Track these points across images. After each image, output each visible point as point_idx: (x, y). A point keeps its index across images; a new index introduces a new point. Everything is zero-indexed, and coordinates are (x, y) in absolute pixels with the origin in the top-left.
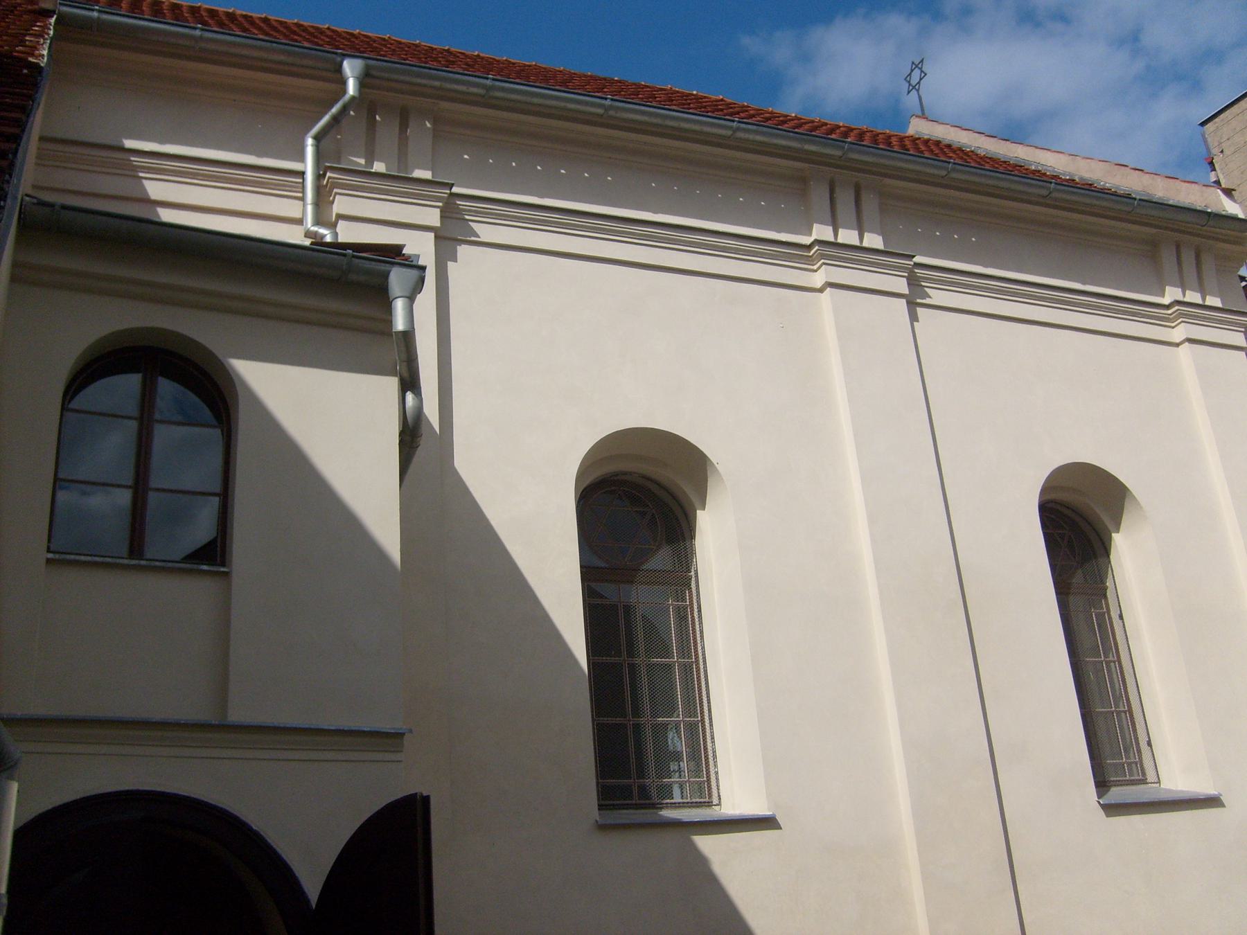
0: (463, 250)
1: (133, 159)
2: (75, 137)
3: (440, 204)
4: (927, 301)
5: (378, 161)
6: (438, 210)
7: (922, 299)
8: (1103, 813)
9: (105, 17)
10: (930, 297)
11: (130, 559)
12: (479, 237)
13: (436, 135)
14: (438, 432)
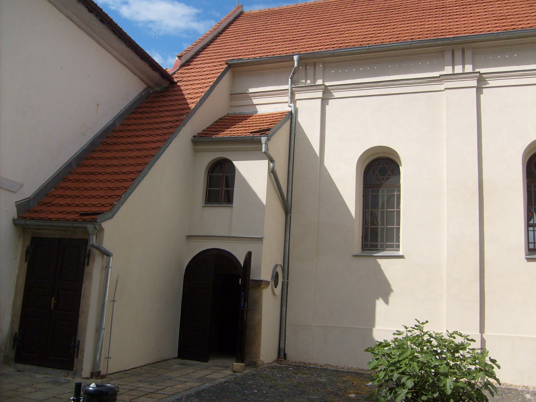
0: (330, 101)
1: (483, 76)
2: (238, 92)
3: (477, 79)
4: (488, 86)
5: (456, 65)
6: (322, 92)
7: (485, 85)
8: (526, 260)
9: (238, 62)
10: (489, 84)
11: (229, 190)
12: (334, 96)
13: (324, 68)
14: (318, 155)
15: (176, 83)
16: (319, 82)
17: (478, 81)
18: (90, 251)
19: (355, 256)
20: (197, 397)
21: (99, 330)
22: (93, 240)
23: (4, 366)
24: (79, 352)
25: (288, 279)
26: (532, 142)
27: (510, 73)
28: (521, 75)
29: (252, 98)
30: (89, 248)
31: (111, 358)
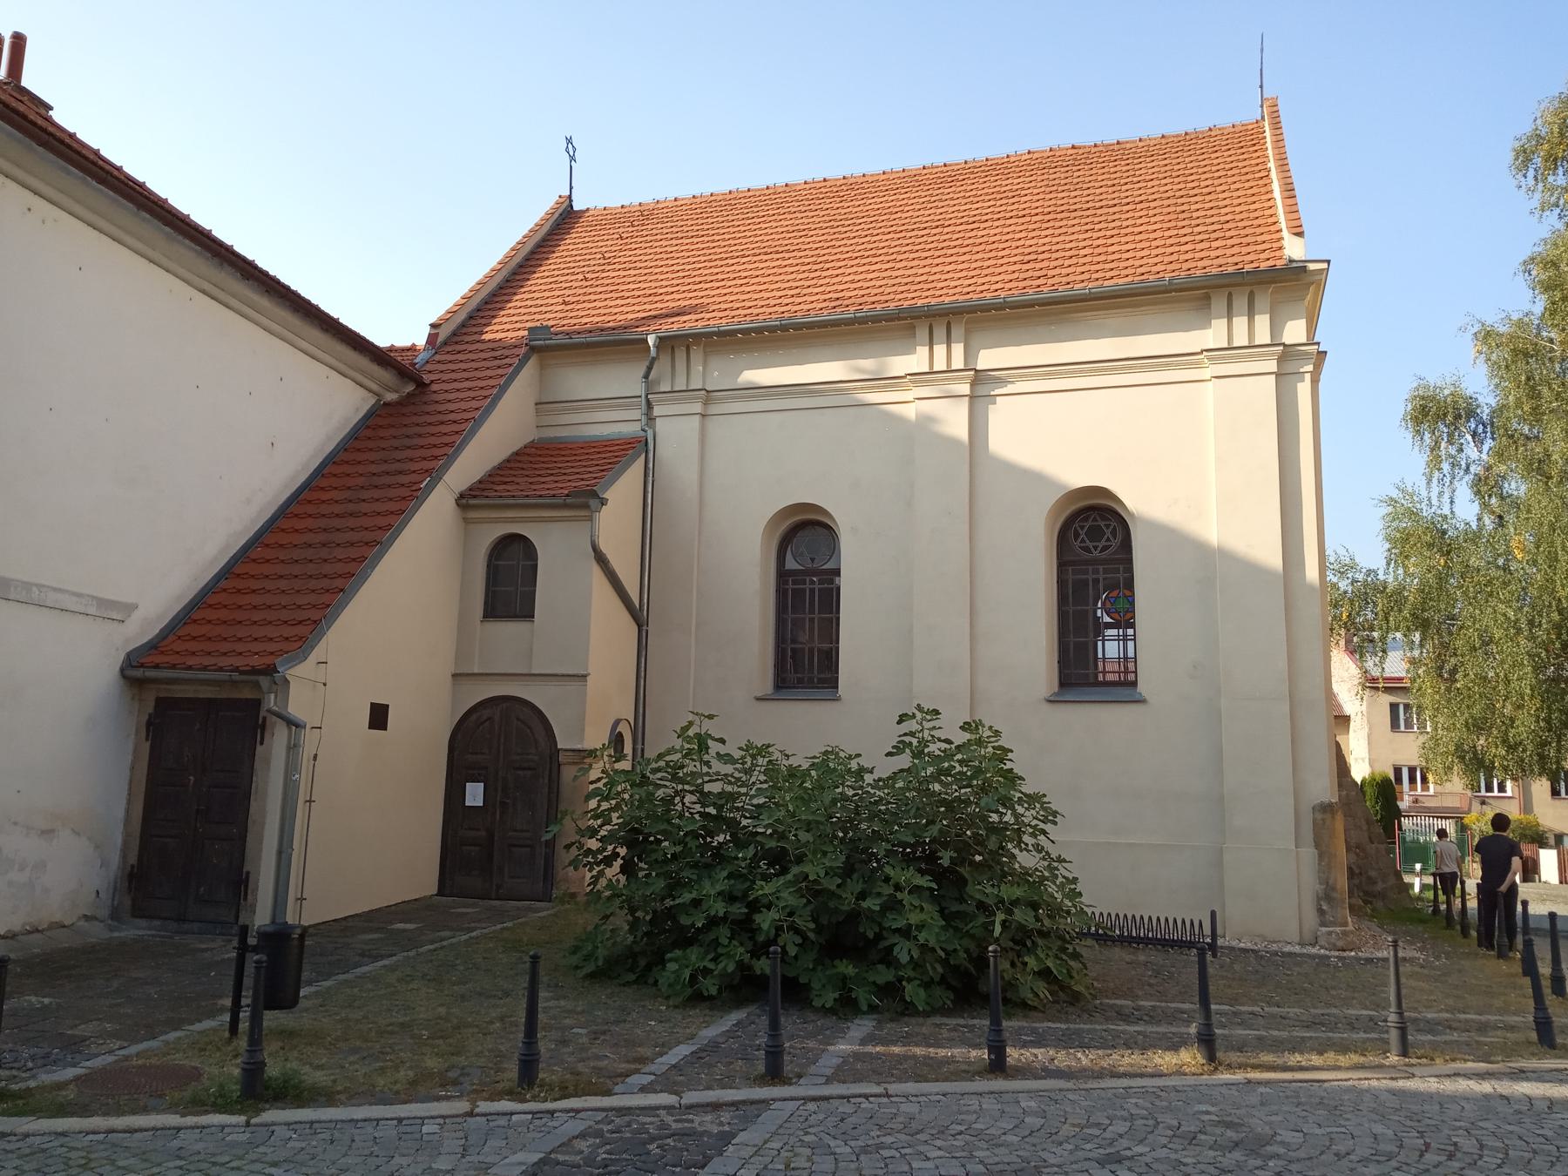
15: (428, 385)
17: (973, 384)
18: (264, 718)
19: (758, 699)
20: (946, 765)
21: (283, 854)
22: (271, 702)
24: (249, 892)
25: (643, 744)
30: (262, 714)
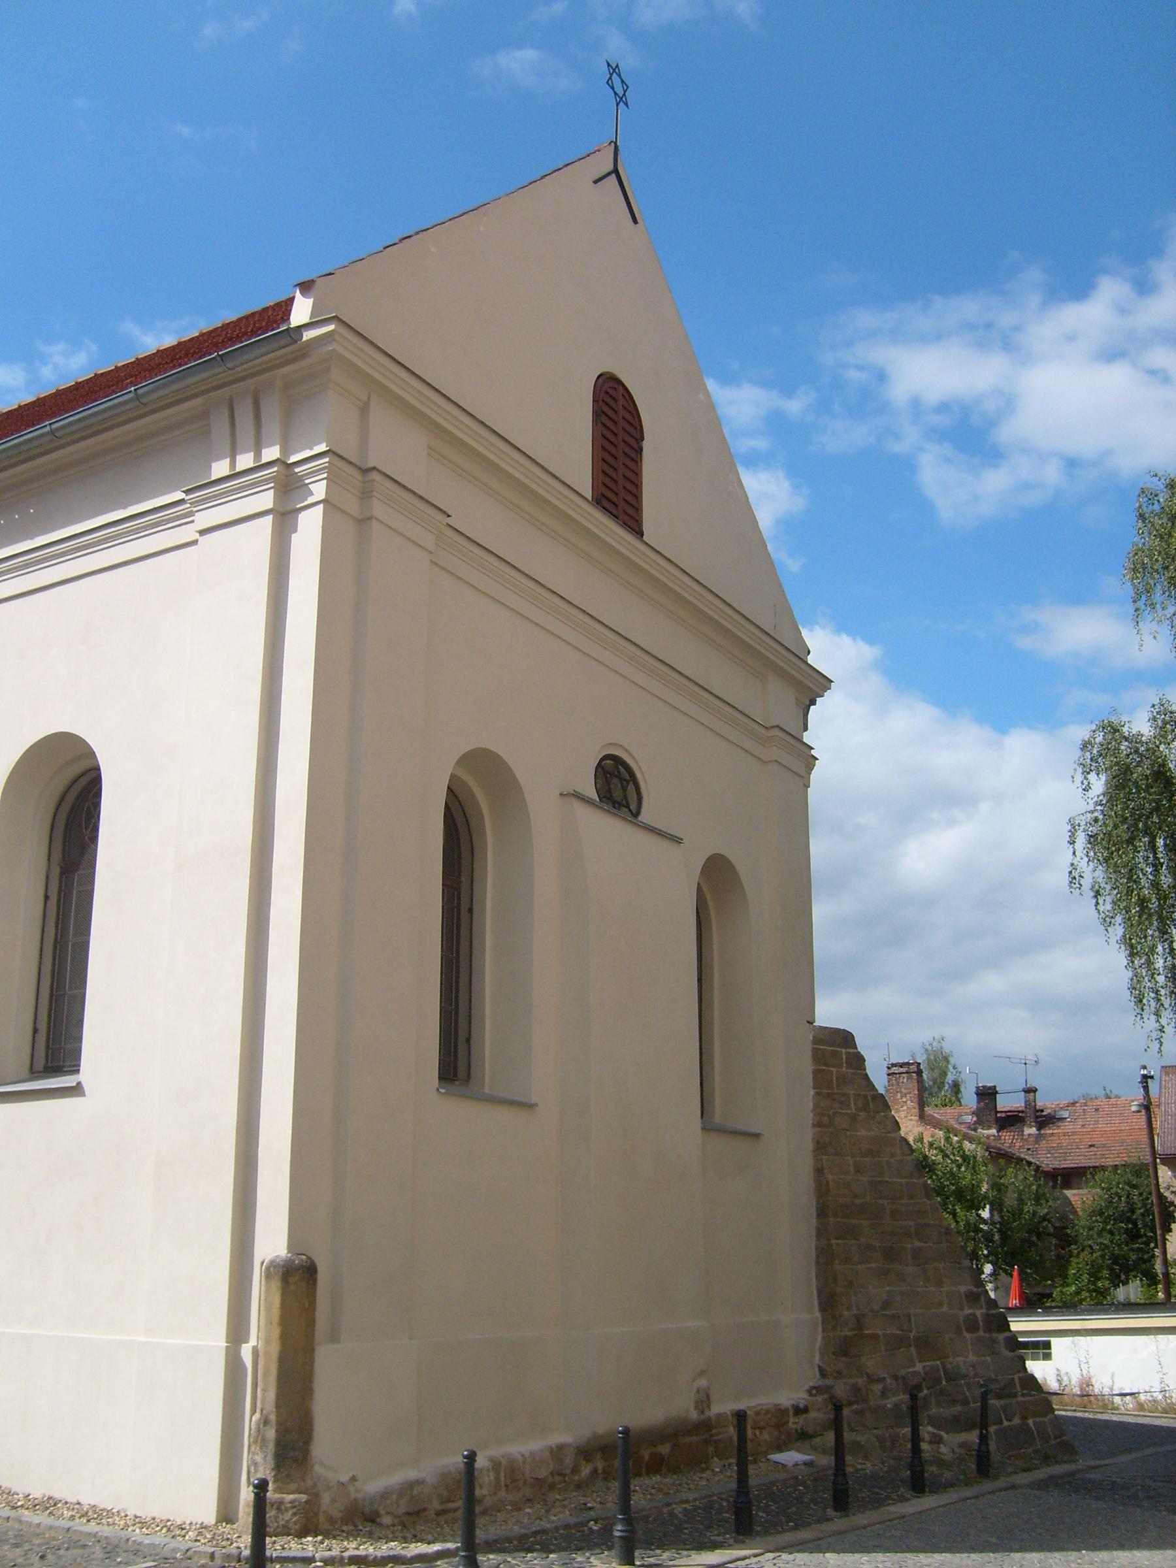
3: (325, 475)
5: (265, 448)
16: (271, 453)
23: (1078, 1210)
26: (25, 753)
27: (107, 529)
28: (24, 565)
29: (307, 482)
31: (1030, 1090)
